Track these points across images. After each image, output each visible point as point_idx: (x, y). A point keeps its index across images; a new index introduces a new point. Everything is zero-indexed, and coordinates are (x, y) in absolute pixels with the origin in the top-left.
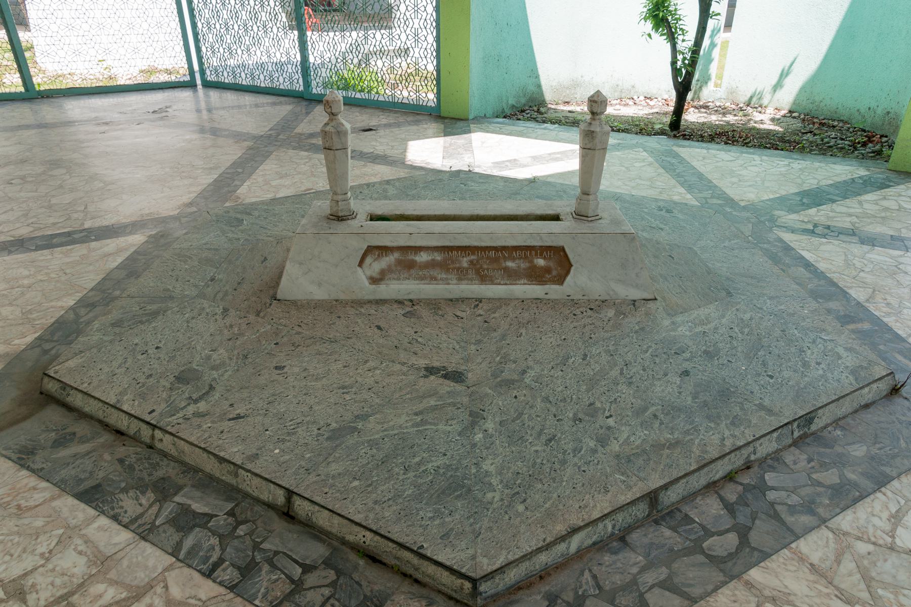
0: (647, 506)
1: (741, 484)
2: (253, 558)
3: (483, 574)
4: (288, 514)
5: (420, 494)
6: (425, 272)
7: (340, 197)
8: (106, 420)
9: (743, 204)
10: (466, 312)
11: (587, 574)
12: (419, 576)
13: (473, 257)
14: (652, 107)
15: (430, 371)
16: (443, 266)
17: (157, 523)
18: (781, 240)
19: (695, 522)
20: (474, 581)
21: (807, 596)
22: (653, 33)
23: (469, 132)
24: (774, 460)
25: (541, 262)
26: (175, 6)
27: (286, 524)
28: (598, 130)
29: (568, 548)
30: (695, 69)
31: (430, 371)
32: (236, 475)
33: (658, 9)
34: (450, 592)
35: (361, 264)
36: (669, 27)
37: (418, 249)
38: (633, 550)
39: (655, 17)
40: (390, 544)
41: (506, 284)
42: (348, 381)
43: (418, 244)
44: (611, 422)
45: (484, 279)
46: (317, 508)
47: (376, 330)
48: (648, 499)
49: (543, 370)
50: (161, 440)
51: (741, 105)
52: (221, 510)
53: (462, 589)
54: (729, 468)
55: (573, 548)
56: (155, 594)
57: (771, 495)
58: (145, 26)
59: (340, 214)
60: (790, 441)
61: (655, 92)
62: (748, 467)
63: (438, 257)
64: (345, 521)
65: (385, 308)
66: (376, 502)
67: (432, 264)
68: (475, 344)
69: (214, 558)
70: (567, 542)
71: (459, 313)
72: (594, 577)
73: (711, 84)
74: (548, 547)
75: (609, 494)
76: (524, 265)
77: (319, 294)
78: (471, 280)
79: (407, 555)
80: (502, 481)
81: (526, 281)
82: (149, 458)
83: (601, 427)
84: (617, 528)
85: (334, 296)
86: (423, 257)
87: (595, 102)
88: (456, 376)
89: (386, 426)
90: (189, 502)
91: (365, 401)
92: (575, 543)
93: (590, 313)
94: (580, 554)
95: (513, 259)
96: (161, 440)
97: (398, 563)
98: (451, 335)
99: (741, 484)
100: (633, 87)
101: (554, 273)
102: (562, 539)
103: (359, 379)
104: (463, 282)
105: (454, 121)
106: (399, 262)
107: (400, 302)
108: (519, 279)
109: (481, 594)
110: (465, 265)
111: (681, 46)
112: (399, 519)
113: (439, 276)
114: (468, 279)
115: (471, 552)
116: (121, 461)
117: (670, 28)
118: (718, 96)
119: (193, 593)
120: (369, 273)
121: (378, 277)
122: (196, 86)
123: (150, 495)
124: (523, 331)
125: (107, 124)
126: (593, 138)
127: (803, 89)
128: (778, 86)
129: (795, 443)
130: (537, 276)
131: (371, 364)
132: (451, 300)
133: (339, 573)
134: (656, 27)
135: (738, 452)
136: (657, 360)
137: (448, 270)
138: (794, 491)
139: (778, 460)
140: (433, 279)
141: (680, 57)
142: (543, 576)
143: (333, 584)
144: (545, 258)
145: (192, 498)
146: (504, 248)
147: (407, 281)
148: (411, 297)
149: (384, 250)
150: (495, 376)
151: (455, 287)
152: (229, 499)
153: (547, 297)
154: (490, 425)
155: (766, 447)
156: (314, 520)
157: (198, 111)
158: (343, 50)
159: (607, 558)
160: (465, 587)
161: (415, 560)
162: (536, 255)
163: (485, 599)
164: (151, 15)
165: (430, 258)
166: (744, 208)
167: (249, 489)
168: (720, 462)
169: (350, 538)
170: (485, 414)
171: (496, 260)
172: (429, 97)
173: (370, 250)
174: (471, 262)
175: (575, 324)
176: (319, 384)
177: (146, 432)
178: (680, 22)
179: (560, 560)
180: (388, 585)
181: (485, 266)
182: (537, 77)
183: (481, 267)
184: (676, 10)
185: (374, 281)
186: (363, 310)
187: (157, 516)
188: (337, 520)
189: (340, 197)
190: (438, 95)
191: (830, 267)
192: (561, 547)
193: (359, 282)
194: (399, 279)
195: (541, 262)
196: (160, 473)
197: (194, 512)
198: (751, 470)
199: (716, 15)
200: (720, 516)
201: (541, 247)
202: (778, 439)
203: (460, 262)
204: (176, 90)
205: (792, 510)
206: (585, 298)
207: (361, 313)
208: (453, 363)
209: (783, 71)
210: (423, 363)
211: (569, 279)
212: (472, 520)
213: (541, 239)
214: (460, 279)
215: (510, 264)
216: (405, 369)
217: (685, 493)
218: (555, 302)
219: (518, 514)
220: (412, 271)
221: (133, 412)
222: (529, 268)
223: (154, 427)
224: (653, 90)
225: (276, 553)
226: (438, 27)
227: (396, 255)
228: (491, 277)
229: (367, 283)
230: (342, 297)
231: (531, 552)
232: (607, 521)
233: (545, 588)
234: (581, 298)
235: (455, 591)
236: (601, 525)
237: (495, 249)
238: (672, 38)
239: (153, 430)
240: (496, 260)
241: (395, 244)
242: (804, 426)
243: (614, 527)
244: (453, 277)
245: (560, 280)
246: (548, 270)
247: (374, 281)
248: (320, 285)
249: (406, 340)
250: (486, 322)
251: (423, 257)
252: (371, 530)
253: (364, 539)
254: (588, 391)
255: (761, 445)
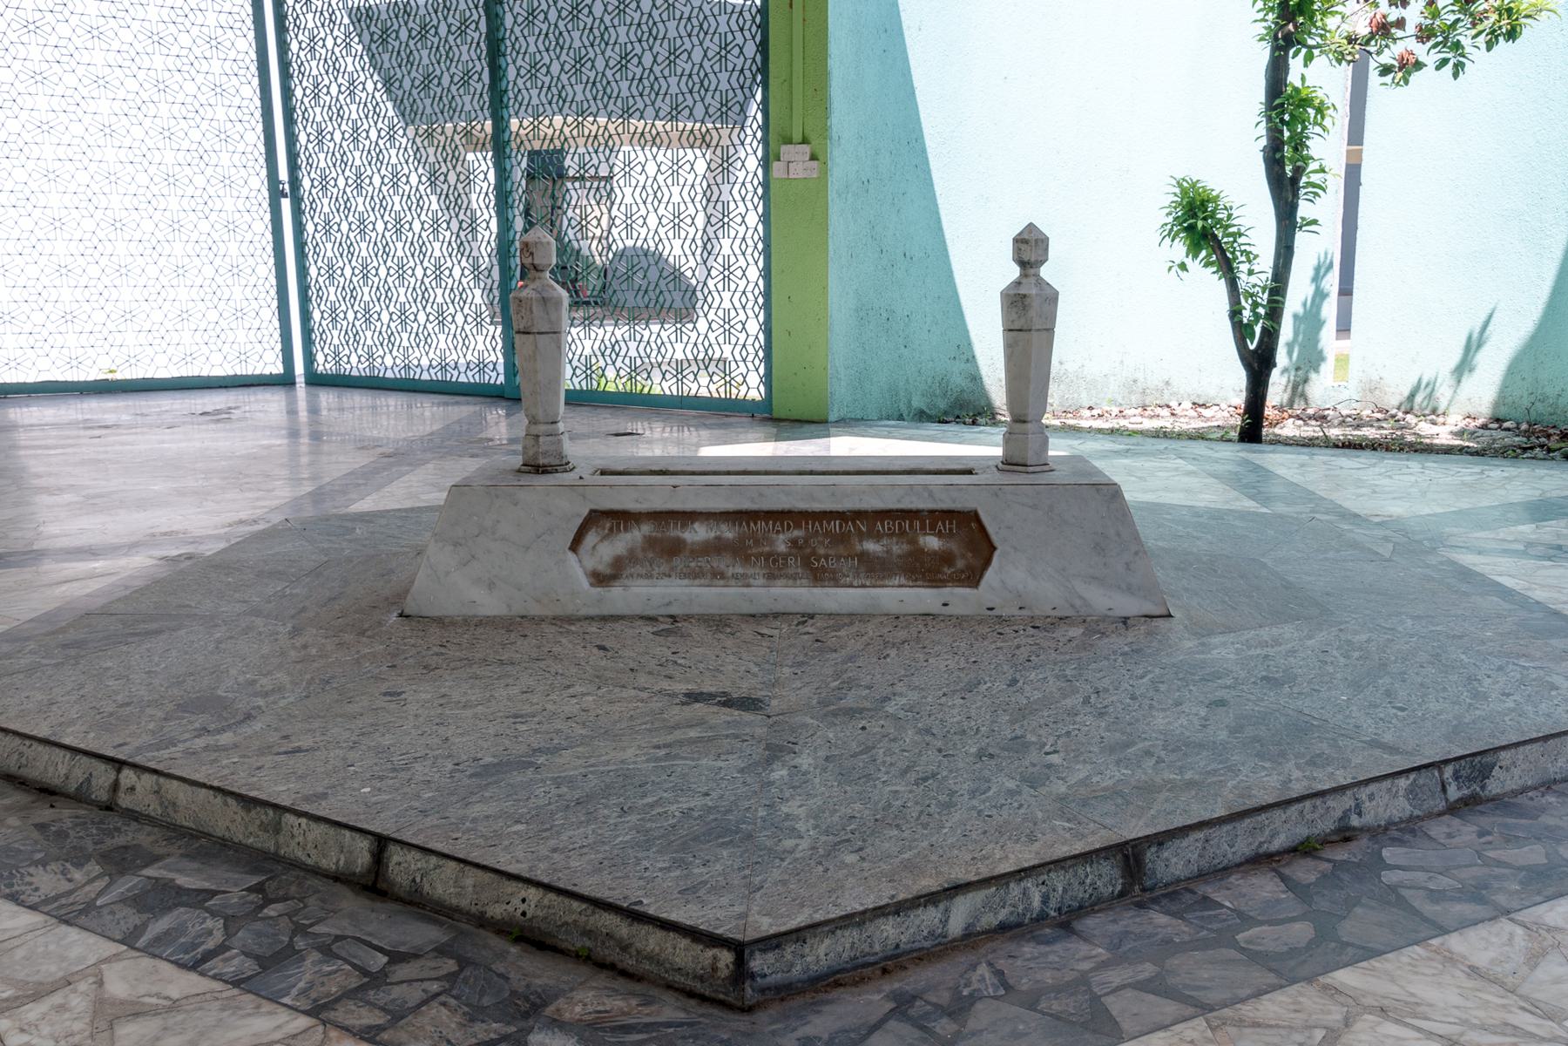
0: (1117, 873)
1: (1329, 861)
2: (291, 945)
3: (757, 936)
4: (373, 884)
5: (647, 841)
6: (702, 562)
7: (542, 428)
8: (24, 772)
9: (1377, 520)
11: (983, 970)
12: (629, 962)
13: (797, 533)
14: (1208, 420)
15: (694, 697)
16: (738, 550)
17: (98, 903)
18: (1453, 563)
19: (1223, 906)
20: (740, 949)
21: (1457, 1007)
22: (1188, 261)
24: (1405, 830)
25: (932, 542)
26: (270, 237)
27: (367, 902)
28: (1034, 291)
29: (945, 922)
30: (1279, 324)
31: (694, 697)
32: (277, 829)
33: (1195, 216)
34: (691, 983)
36: (1218, 248)
38: (1085, 940)
39: (1191, 229)
40: (575, 904)
41: (863, 586)
42: (527, 709)
43: (689, 506)
44: (1055, 759)
45: (819, 576)
46: (434, 860)
47: (595, 650)
48: (1119, 857)
50: (133, 789)
51: (1394, 412)
52: (236, 885)
53: (714, 969)
54: (1302, 832)
55: (956, 927)
56: (75, 991)
57: (1389, 877)
58: (208, 271)
59: (541, 461)
60: (1442, 805)
61: (1212, 393)
62: (1345, 835)
63: (728, 532)
64: (488, 876)
65: (618, 626)
66: (555, 850)
67: (716, 548)
69: (210, 944)
70: (942, 906)
71: (765, 631)
72: (999, 973)
73: (1327, 368)
74: (898, 909)
75: (1037, 844)
76: (898, 548)
77: (490, 604)
78: (794, 577)
79: (608, 921)
80: (816, 827)
81: (903, 581)
82: (102, 822)
83: (1034, 765)
84: (1053, 904)
85: (518, 609)
86: (699, 533)
87: (1025, 242)
88: (749, 704)
89: (592, 761)
90: (171, 875)
91: (558, 732)
92: (959, 915)
93: (1032, 631)
94: (971, 939)
95: (878, 537)
96: (133, 789)
97: (588, 944)
98: (744, 656)
99: (1329, 861)
100: (1167, 383)
101: (960, 564)
102: (931, 899)
103: (549, 706)
104: (778, 582)
106: (650, 543)
107: (651, 619)
108: (890, 577)
109: (753, 976)
110: (782, 548)
111: (1244, 281)
112: (600, 870)
113: (730, 571)
114: (787, 577)
115: (738, 909)
116: (42, 827)
117: (1223, 252)
118: (1345, 395)
119: (154, 989)
120: (590, 564)
121: (608, 571)
122: (293, 383)
123: (94, 868)
124: (893, 653)
125: (106, 427)
126: (1025, 308)
127: (1513, 370)
128: (1464, 367)
129: (1453, 809)
130: (925, 570)
131: (578, 689)
133: (463, 963)
134: (1194, 249)
135: (1318, 802)
136: (1163, 687)
137: (746, 559)
138: (1444, 872)
139: (1413, 832)
140: (718, 575)
141: (1246, 304)
142: (892, 963)
143: (451, 977)
144: (940, 535)
145: (178, 871)
146: (858, 515)
147: (666, 581)
148: (674, 610)
149: (621, 518)
150: (823, 703)
152: (255, 871)
154: (805, 761)
155: (1385, 805)
156: (427, 888)
157: (294, 434)
158: (588, 351)
159: (1028, 949)
160: (721, 965)
161: (623, 929)
162: (923, 528)
163: (763, 991)
164: (221, 253)
165: (712, 535)
166: (1379, 524)
167: (300, 854)
168: (1278, 815)
169: (496, 911)
170: (797, 748)
171: (843, 539)
172: (753, 389)
173: (596, 518)
176: (469, 713)
177: (103, 776)
178: (1241, 240)
179: (927, 944)
180: (565, 978)
181: (822, 551)
182: (972, 359)
183: (814, 553)
184: (1230, 216)
187: (100, 894)
188: (471, 878)
189: (542, 428)
190: (768, 380)
191: (1556, 595)
192: (929, 917)
193: (570, 580)
194: (649, 576)
195: (932, 542)
196: (120, 840)
197: (179, 887)
198: (1353, 844)
199: (1309, 223)
200: (1278, 901)
201: (932, 512)
202: (1411, 792)
203: (771, 543)
204: (253, 389)
205: (1436, 896)
206: (1023, 612)
207: (568, 632)
208: (743, 688)
209: (1470, 338)
210: (682, 687)
211: (990, 575)
212: (747, 872)
213: (931, 495)
214: (771, 577)
215: (871, 546)
216: (644, 695)
217: (1204, 863)
218: (960, 621)
219: (844, 865)
220: (678, 562)
221: (82, 746)
222: (910, 554)
223: (119, 764)
224: (1208, 391)
225: (338, 938)
226: (767, 253)
227: (646, 529)
228: (834, 572)
229: (585, 582)
230: (536, 610)
231: (864, 912)
232: (1029, 883)
233: (894, 984)
234: (1017, 612)
235: (701, 979)
236: (1015, 889)
238: (1227, 268)
239: (119, 771)
240: (843, 539)
242: (1469, 779)
243: (1045, 900)
244: (757, 571)
245: (972, 578)
246: (946, 558)
247: (600, 579)
248: (491, 586)
249: (654, 662)
251: (699, 533)
252: (538, 884)
253: (523, 907)
254: (1013, 722)
255: (1371, 797)
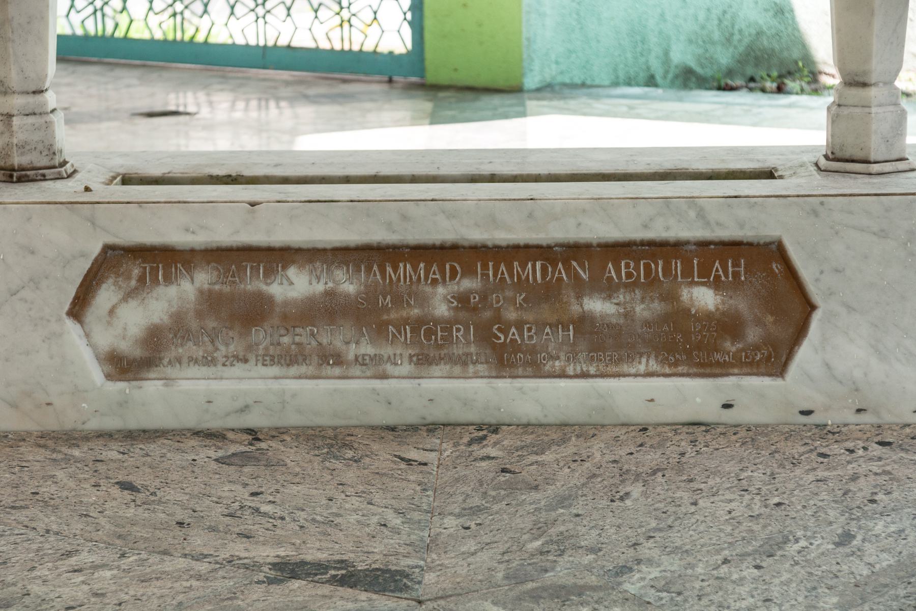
6: (303, 335)
10: (437, 453)
13: (467, 284)
16: (366, 315)
23: (523, 114)
25: (704, 298)
35: (78, 308)
37: (278, 257)
41: (584, 375)
45: (507, 359)
49: (691, 566)
59: (17, 160)
63: (348, 285)
67: (325, 310)
68: (459, 516)
71: (413, 454)
76: (645, 309)
78: (464, 361)
81: (654, 365)
86: (296, 285)
93: (877, 450)
95: (608, 290)
101: (753, 334)
104: (436, 370)
105: (469, 95)
106: (211, 302)
108: (630, 359)
110: (442, 310)
113: (352, 351)
114: (452, 360)
120: (106, 339)
121: (138, 353)
130: (692, 347)
131: (85, 558)
132: (393, 429)
137: (380, 331)
140: (331, 359)
144: (717, 285)
146: (575, 250)
147: (238, 369)
148: (253, 420)
149: (157, 261)
150: (514, 578)
151: (406, 384)
153: (728, 416)
165: (320, 288)
171: (548, 293)
173: (113, 260)
174: (463, 300)
175: (821, 474)
181: (511, 315)
183: (498, 318)
185: (122, 366)
186: (76, 453)
194: (209, 361)
195: (704, 298)
201: (703, 244)
203: (423, 301)
207: (68, 459)
208: (376, 553)
210: (268, 553)
211: (805, 353)
213: (701, 214)
214: (423, 361)
215: (597, 306)
216: (203, 567)
218: (753, 435)
220: (259, 335)
222: (665, 318)
227: (203, 278)
228: (533, 351)
229: (96, 373)
234: (852, 418)
237: (544, 253)
240: (548, 293)
241: (199, 239)
244: (398, 351)
245: (775, 359)
246: (728, 325)
247: (122, 366)
250: (504, 471)
251: (296, 285)
